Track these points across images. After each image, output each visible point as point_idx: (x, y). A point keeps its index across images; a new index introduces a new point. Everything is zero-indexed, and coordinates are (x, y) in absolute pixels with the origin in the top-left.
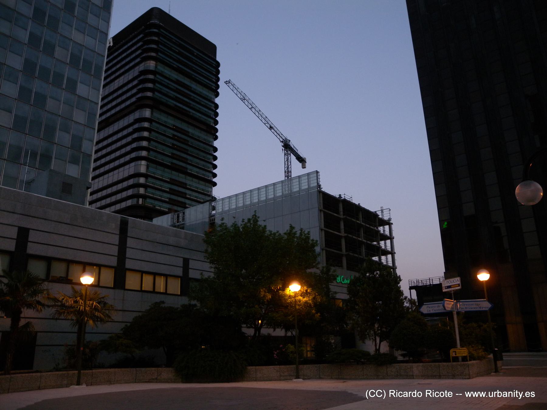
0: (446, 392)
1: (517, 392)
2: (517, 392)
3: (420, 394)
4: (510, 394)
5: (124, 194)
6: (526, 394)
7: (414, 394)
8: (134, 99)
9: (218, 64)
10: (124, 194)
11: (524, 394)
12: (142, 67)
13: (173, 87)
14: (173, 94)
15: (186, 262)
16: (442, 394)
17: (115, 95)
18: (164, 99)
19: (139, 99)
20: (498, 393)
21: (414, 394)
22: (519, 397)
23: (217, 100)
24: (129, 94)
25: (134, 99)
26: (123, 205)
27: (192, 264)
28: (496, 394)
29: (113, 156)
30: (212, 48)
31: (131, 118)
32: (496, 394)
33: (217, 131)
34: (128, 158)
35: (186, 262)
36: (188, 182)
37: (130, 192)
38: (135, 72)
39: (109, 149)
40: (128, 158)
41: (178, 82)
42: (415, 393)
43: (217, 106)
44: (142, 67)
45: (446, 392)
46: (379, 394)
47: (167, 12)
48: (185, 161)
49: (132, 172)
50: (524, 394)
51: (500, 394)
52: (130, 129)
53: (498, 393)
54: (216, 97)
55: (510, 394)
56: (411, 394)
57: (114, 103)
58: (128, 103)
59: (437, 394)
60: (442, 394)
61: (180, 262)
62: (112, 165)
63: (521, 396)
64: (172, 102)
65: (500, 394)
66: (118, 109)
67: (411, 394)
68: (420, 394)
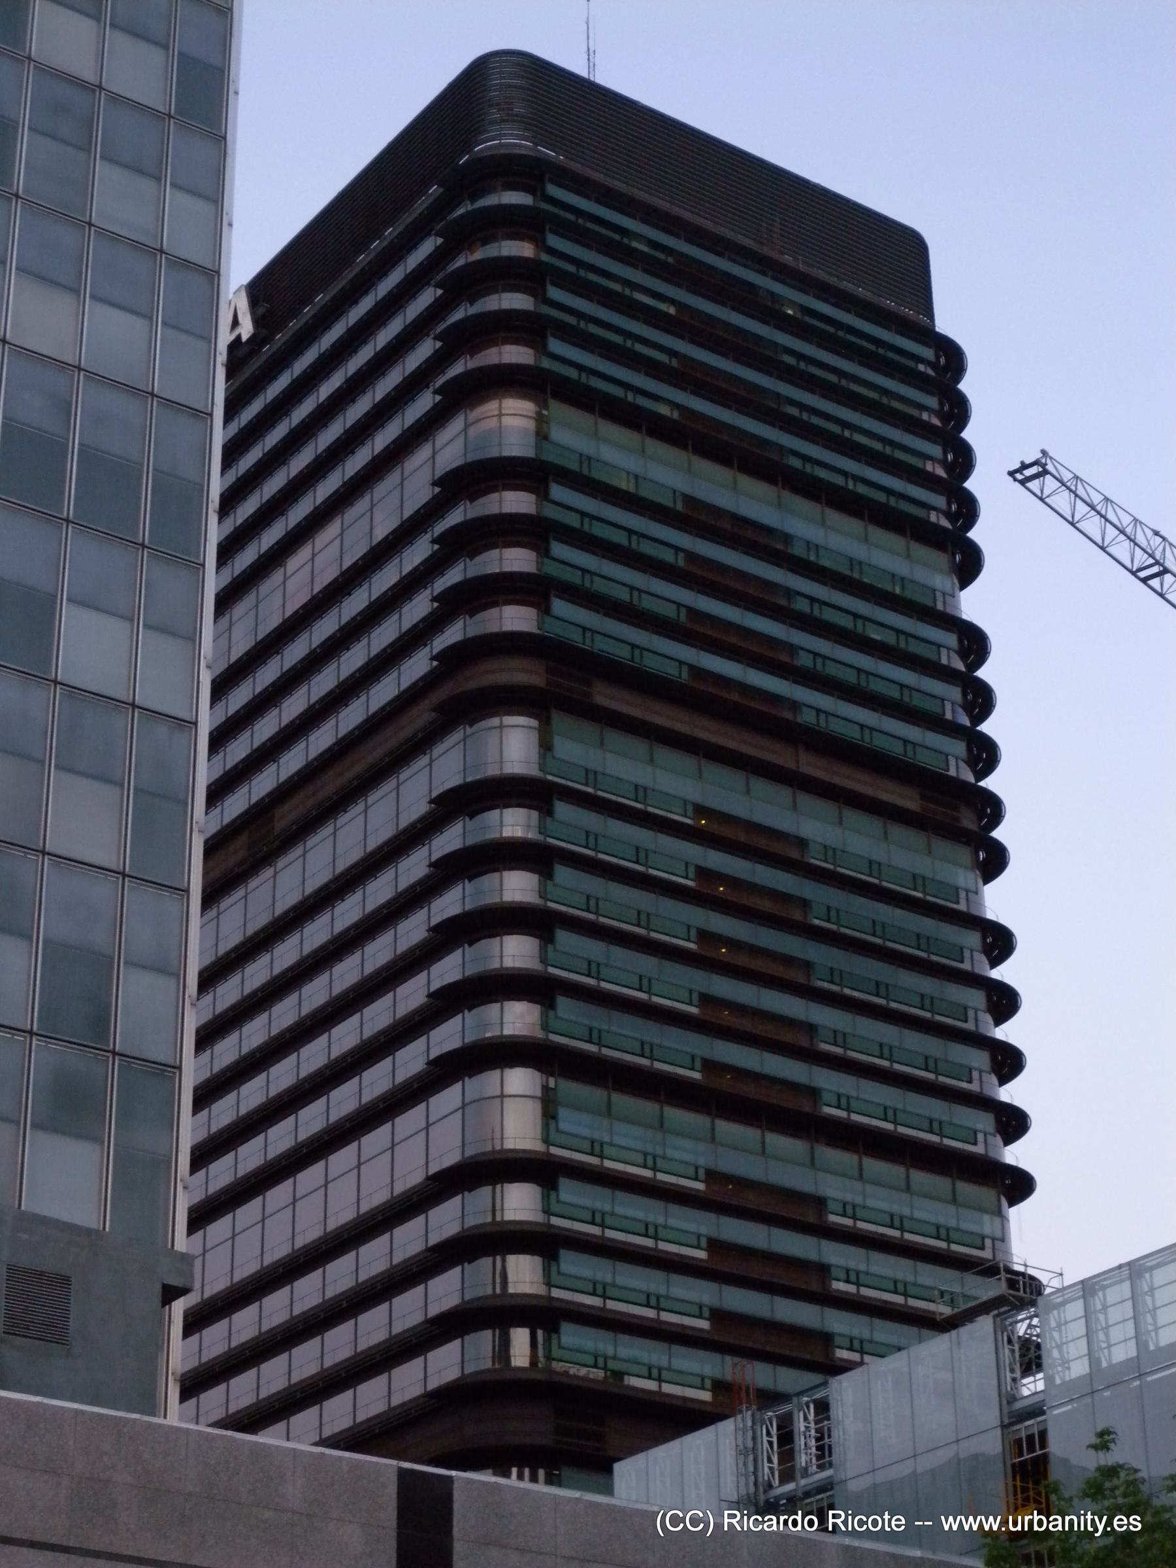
0: (886, 1517)
1: (1089, 1517)
2: (1089, 1517)
3: (811, 1523)
4: (1071, 1521)
5: (408, 1310)
6: (1115, 1523)
7: (795, 1523)
8: (417, 666)
9: (952, 359)
10: (408, 1310)
11: (1109, 1523)
12: (449, 449)
16: (875, 1523)
18: (616, 638)
19: (454, 660)
20: (1036, 1518)
21: (795, 1523)
22: (1096, 1530)
23: (973, 604)
25: (417, 666)
26: (408, 1382)
28: (1031, 1522)
32: (1031, 1522)
33: (992, 809)
34: (411, 1060)
36: (833, 1188)
37: (445, 1291)
40: (411, 1060)
41: (694, 516)
42: (799, 1518)
43: (975, 644)
44: (449, 449)
45: (886, 1517)
46: (695, 1521)
49: (447, 1155)
50: (1109, 1523)
51: (1040, 1523)
52: (413, 867)
53: (1036, 1518)
54: (964, 585)
55: (1071, 1521)
56: (786, 1522)
58: (383, 692)
59: (861, 1523)
60: (875, 1523)
63: (1101, 1528)
64: (671, 656)
65: (1040, 1523)
67: (786, 1522)
68: (811, 1523)
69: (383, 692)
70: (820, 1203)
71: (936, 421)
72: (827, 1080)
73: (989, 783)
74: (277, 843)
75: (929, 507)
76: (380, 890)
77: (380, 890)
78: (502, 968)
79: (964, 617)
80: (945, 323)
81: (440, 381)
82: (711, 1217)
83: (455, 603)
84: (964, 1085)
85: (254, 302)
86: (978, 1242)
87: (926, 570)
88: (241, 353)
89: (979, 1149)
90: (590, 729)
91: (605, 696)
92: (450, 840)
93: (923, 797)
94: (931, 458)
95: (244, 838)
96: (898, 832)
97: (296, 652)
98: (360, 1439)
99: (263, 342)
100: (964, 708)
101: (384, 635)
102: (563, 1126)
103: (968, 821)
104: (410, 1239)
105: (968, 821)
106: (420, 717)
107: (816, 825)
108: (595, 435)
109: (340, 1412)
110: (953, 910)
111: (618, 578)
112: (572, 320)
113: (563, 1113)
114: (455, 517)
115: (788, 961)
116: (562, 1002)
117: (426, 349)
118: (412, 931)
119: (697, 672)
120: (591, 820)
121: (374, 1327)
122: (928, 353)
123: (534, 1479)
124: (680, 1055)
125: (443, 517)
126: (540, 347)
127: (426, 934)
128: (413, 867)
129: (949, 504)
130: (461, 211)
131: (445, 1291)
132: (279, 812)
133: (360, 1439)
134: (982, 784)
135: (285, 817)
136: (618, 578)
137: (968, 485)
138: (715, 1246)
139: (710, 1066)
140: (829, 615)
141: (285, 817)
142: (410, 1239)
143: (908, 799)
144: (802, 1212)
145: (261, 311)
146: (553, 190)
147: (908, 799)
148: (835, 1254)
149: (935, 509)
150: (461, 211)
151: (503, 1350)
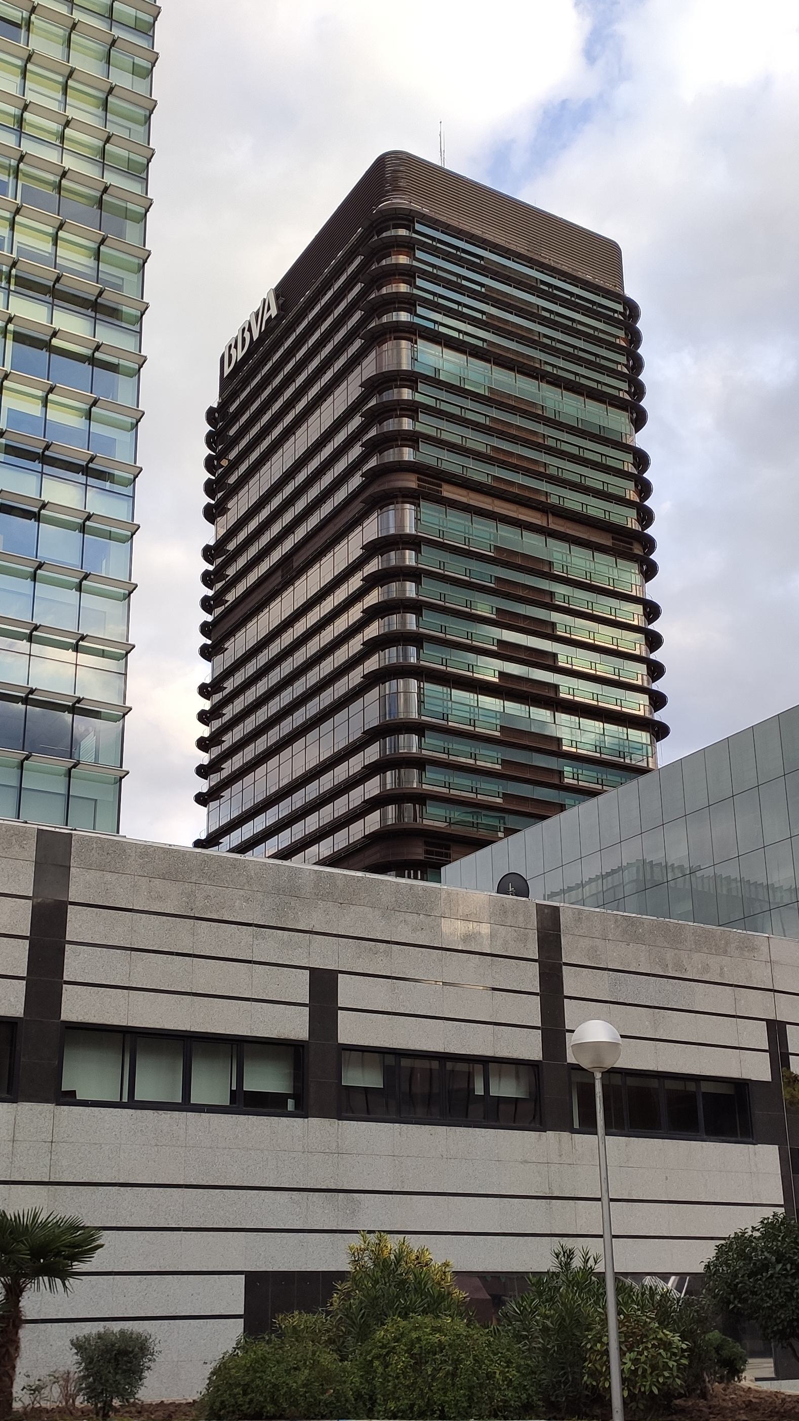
5: (357, 796)
8: (356, 481)
9: (632, 310)
10: (357, 796)
12: (368, 368)
13: (481, 420)
14: (479, 442)
15: (323, 983)
17: (289, 489)
18: (451, 463)
19: (372, 477)
23: (641, 440)
24: (341, 466)
25: (356, 481)
26: (357, 831)
27: (348, 991)
29: (274, 706)
30: (608, 253)
31: (349, 549)
33: (649, 544)
34: (355, 677)
35: (323, 983)
36: (564, 734)
37: (372, 788)
38: (349, 392)
39: (262, 687)
40: (355, 677)
41: (493, 400)
43: (642, 460)
44: (368, 368)
47: (435, 160)
48: (548, 662)
49: (373, 721)
52: (356, 582)
54: (637, 430)
57: (276, 529)
58: (341, 495)
61: (299, 987)
62: (261, 744)
64: (480, 473)
66: (301, 533)
69: (341, 495)
71: (623, 344)
73: (649, 531)
74: (294, 574)
75: (615, 311)
76: (341, 595)
77: (341, 595)
80: (630, 291)
81: (365, 469)
83: (372, 448)
84: (635, 682)
85: (277, 298)
88: (274, 323)
91: (449, 492)
92: (373, 567)
93: (613, 538)
94: (618, 337)
95: (279, 573)
97: (298, 800)
98: (334, 861)
99: (283, 318)
100: (638, 520)
101: (341, 466)
103: (638, 550)
104: (355, 764)
105: (638, 550)
106: (357, 507)
109: (325, 848)
110: (630, 624)
112: (430, 297)
114: (373, 463)
117: (356, 451)
118: (355, 645)
121: (340, 806)
122: (620, 308)
123: (416, 878)
125: (367, 433)
126: (412, 284)
127: (361, 552)
128: (356, 582)
129: (628, 360)
130: (373, 325)
131: (372, 788)
132: (295, 558)
133: (334, 861)
135: (298, 561)
136: (452, 433)
137: (639, 351)
139: (502, 675)
140: (565, 447)
141: (298, 561)
142: (355, 764)
143: (607, 541)
144: (540, 568)
145: (281, 302)
146: (418, 227)
147: (607, 541)
149: (620, 363)
150: (373, 325)
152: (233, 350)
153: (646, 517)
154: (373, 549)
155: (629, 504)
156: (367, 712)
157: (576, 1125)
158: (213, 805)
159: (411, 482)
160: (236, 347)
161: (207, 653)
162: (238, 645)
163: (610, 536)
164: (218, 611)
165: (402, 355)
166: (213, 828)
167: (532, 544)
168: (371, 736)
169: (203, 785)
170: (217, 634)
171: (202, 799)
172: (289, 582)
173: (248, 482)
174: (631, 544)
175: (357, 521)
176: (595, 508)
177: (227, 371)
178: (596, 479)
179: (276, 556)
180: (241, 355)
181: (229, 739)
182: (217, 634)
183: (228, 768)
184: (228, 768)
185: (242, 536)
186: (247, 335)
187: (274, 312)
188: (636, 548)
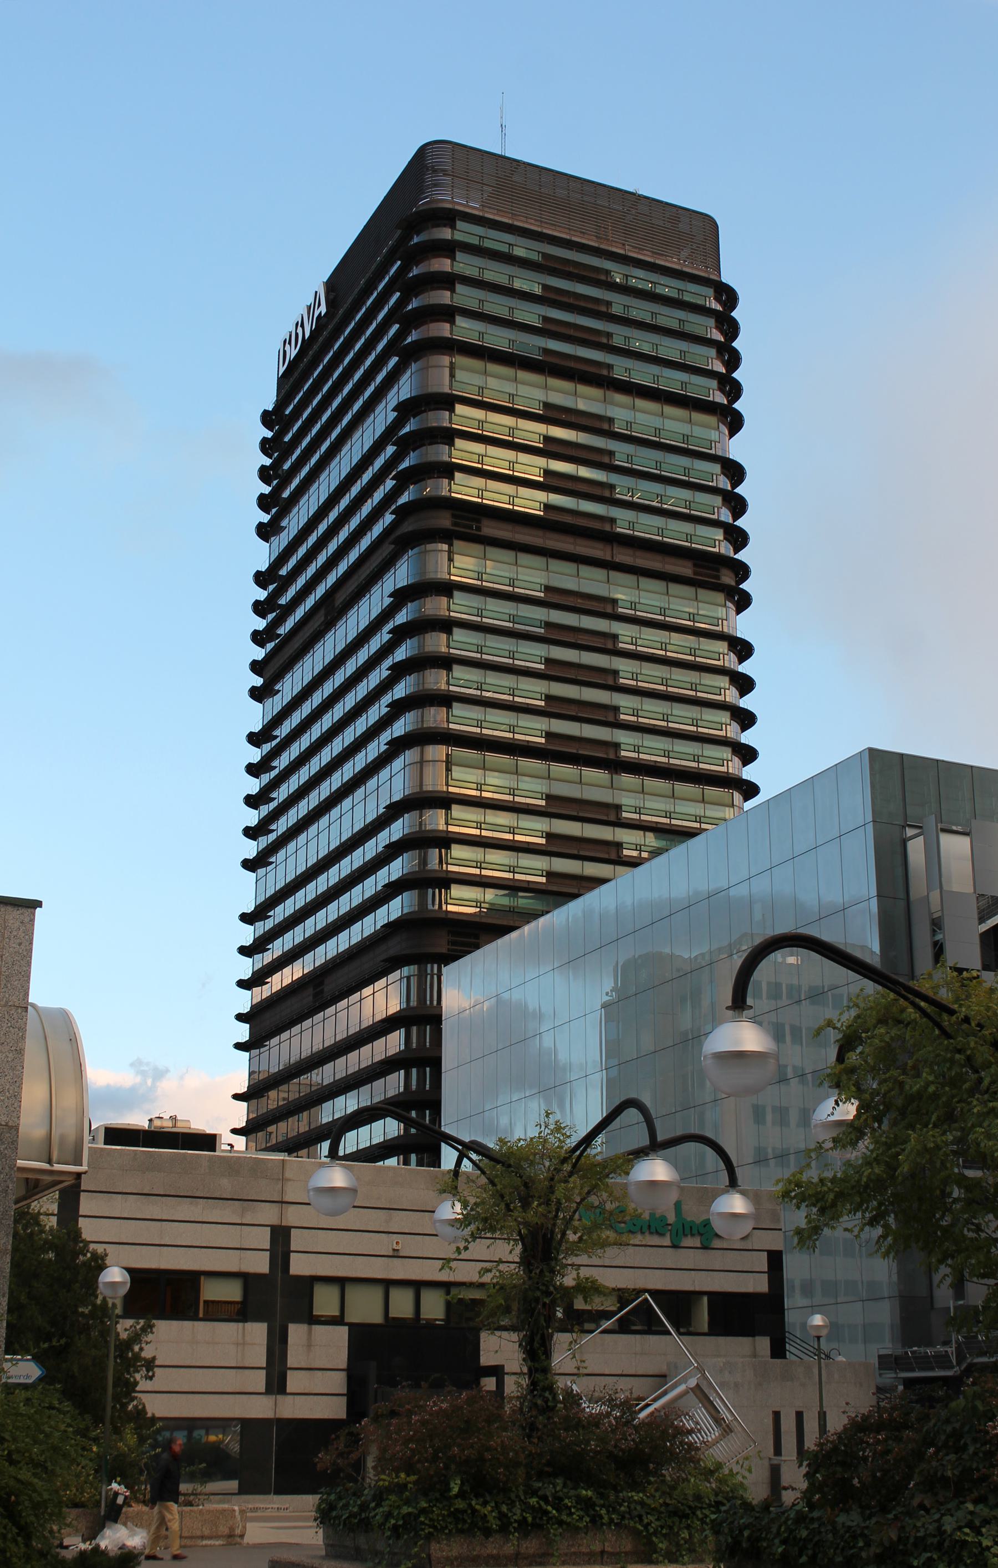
5: (369, 887)
10: (369, 887)
12: (404, 389)
33: (743, 571)
34: (373, 750)
37: (396, 869)
40: (373, 750)
52: (383, 636)
70: (618, 808)
72: (622, 737)
78: (424, 690)
79: (731, 457)
82: (545, 683)
83: (405, 480)
86: (715, 622)
87: (705, 430)
89: (716, 550)
90: (477, 549)
95: (322, 612)
96: (675, 588)
102: (456, 564)
103: (728, 578)
104: (371, 849)
105: (728, 578)
107: (623, 592)
108: (485, 373)
111: (496, 273)
113: (456, 557)
115: (597, 301)
116: (456, 631)
119: (546, 351)
120: (478, 326)
124: (532, 731)
128: (383, 636)
131: (396, 869)
134: (738, 523)
135: (340, 598)
136: (496, 273)
138: (549, 698)
141: (340, 598)
143: (685, 569)
144: (605, 608)
145: (331, 297)
148: (623, 666)
151: (424, 861)
152: (287, 346)
153: (739, 538)
154: (401, 597)
155: (716, 524)
156: (394, 783)
157: (201, 1315)
158: (261, 871)
159: (444, 521)
160: (290, 343)
161: (257, 694)
162: (290, 686)
163: (689, 564)
164: (270, 646)
165: (441, 374)
166: (261, 899)
167: (591, 581)
168: (394, 811)
169: (251, 849)
170: (270, 670)
171: (249, 865)
172: (330, 624)
173: (298, 502)
174: (718, 571)
175: (388, 564)
176: (676, 533)
177: (282, 370)
178: (675, 498)
179: (320, 590)
180: (294, 353)
181: (282, 793)
182: (270, 670)
183: (282, 825)
184: (282, 825)
185: (292, 562)
186: (300, 330)
187: (323, 309)
188: (724, 577)
